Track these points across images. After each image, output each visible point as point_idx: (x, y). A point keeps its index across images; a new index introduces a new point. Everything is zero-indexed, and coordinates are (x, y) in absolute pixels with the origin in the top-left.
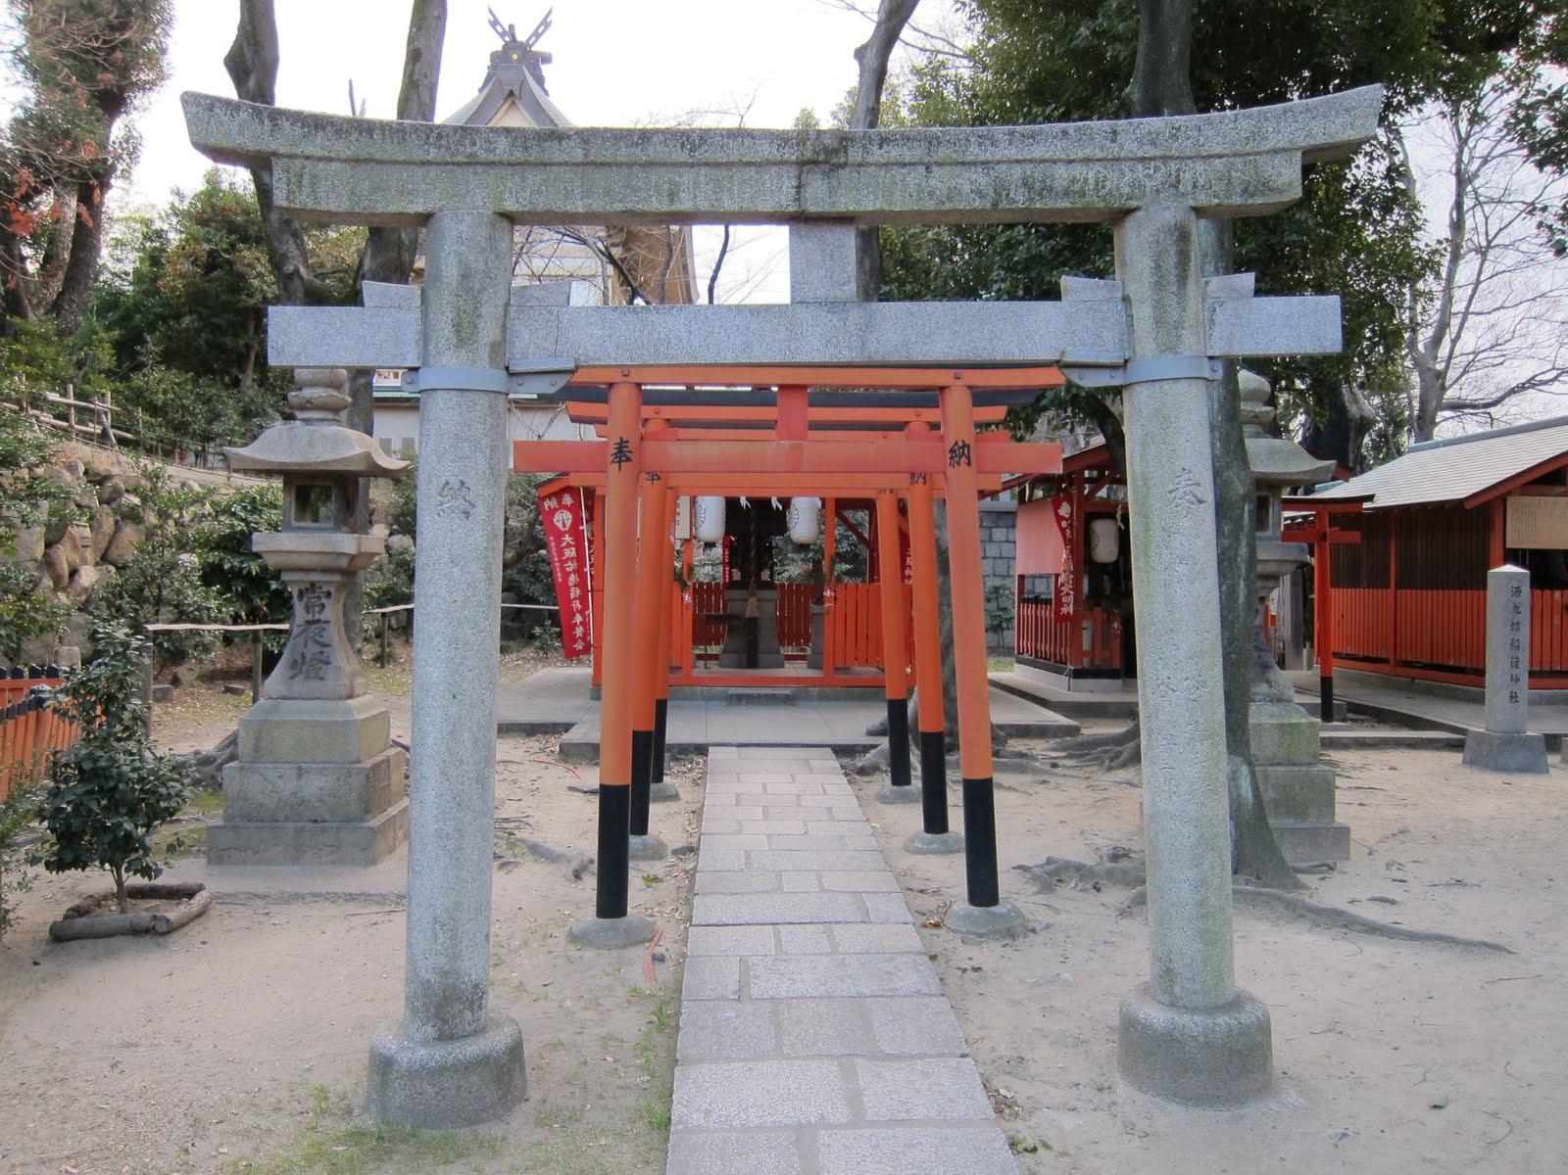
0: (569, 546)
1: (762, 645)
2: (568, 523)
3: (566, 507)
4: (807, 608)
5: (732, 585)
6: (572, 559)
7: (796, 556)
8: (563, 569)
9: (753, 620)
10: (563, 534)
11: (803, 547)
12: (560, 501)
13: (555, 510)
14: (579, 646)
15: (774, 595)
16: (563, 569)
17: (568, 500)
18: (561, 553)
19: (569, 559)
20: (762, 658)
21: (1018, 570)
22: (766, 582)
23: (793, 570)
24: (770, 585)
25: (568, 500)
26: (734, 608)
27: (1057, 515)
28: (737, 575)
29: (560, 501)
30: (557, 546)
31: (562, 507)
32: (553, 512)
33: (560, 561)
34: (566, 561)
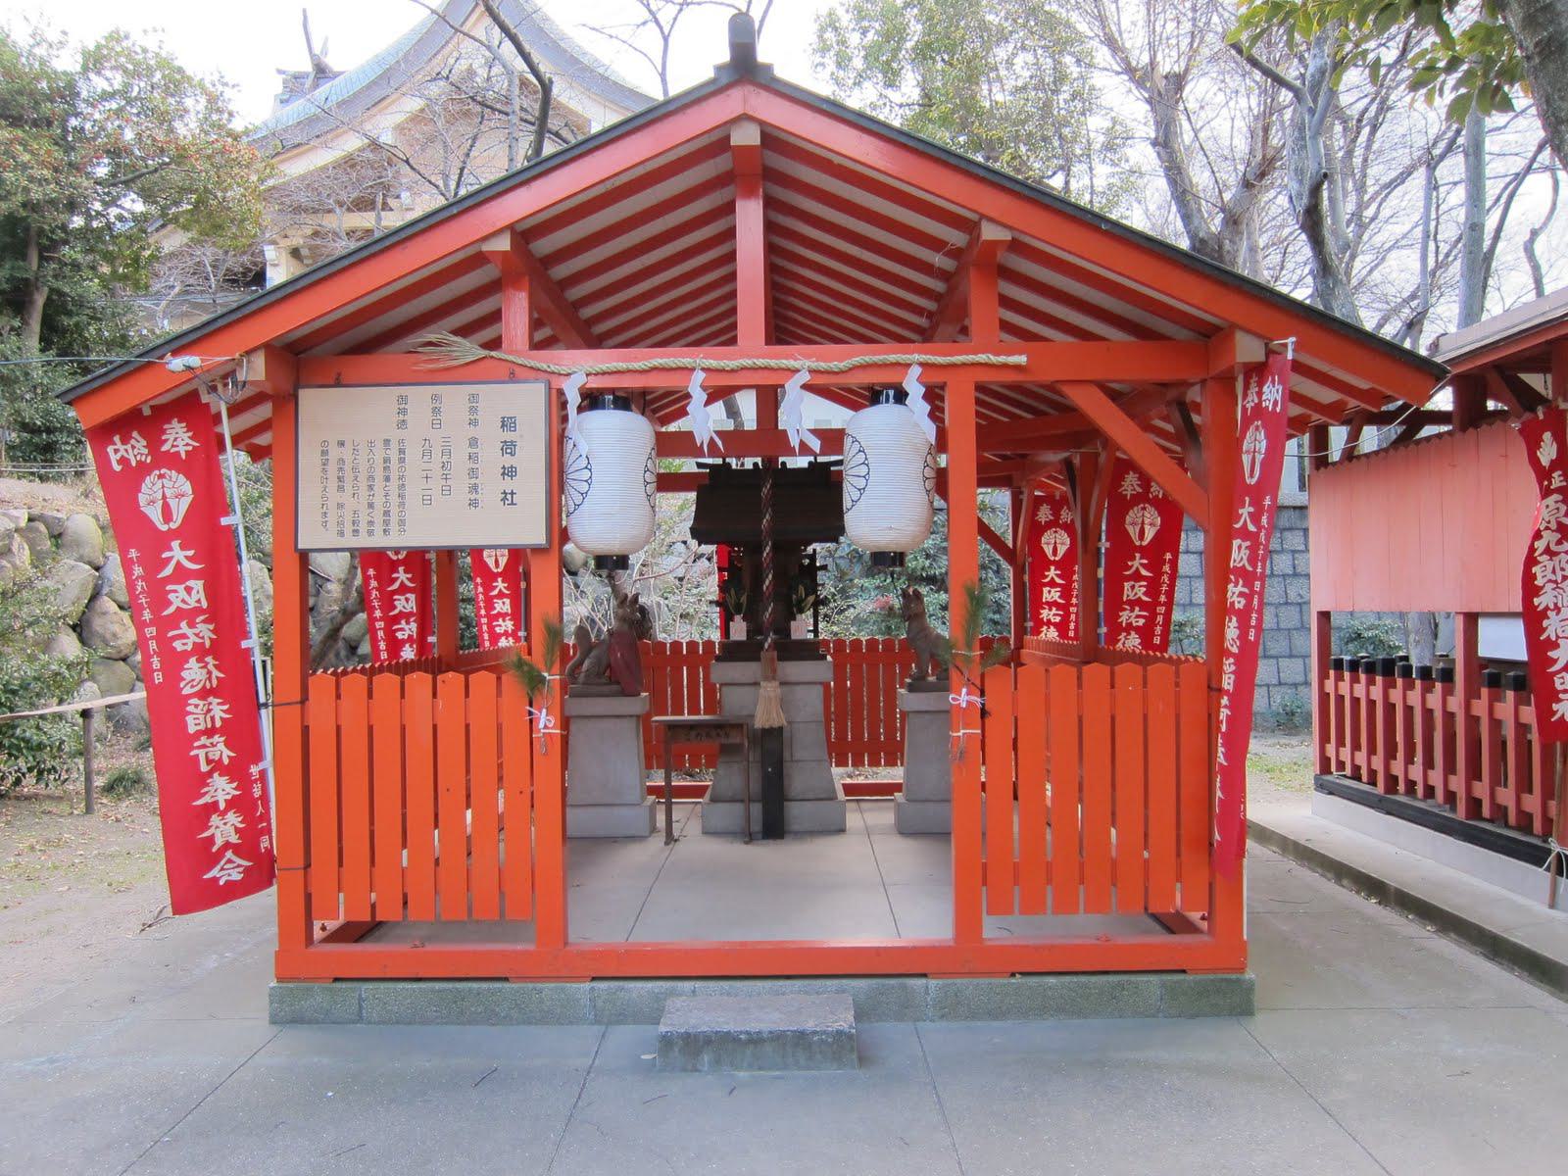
0: (501, 595)
1: (798, 780)
2: (180, 508)
3: (172, 461)
4: (891, 697)
5: (732, 652)
6: (190, 615)
7: (867, 582)
8: (491, 629)
9: (774, 734)
10: (163, 540)
11: (885, 561)
12: (154, 444)
13: (143, 470)
14: (229, 871)
15: (821, 671)
16: (491, 629)
17: (178, 438)
18: (388, 603)
19: (403, 615)
20: (797, 812)
21: (1318, 604)
22: (804, 643)
23: (858, 612)
24: (810, 651)
25: (178, 438)
26: (734, 702)
27: (1534, 462)
28: (739, 630)
29: (154, 444)
30: (485, 594)
31: (163, 460)
32: (135, 475)
33: (488, 616)
34: (396, 619)
